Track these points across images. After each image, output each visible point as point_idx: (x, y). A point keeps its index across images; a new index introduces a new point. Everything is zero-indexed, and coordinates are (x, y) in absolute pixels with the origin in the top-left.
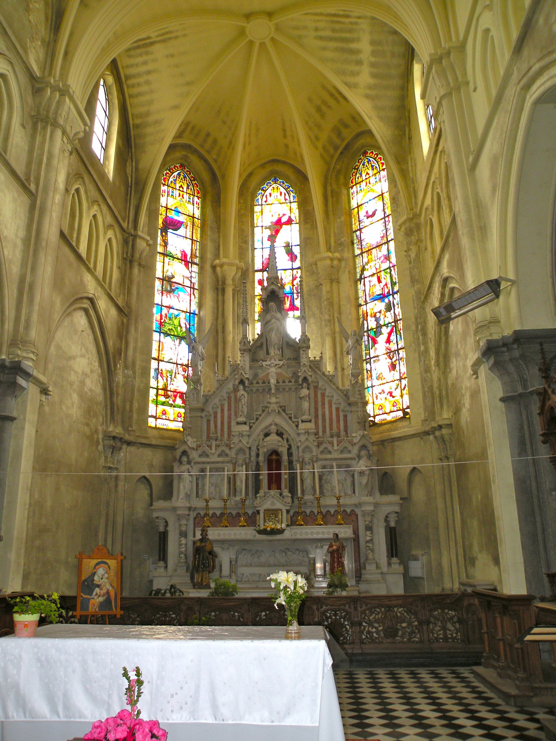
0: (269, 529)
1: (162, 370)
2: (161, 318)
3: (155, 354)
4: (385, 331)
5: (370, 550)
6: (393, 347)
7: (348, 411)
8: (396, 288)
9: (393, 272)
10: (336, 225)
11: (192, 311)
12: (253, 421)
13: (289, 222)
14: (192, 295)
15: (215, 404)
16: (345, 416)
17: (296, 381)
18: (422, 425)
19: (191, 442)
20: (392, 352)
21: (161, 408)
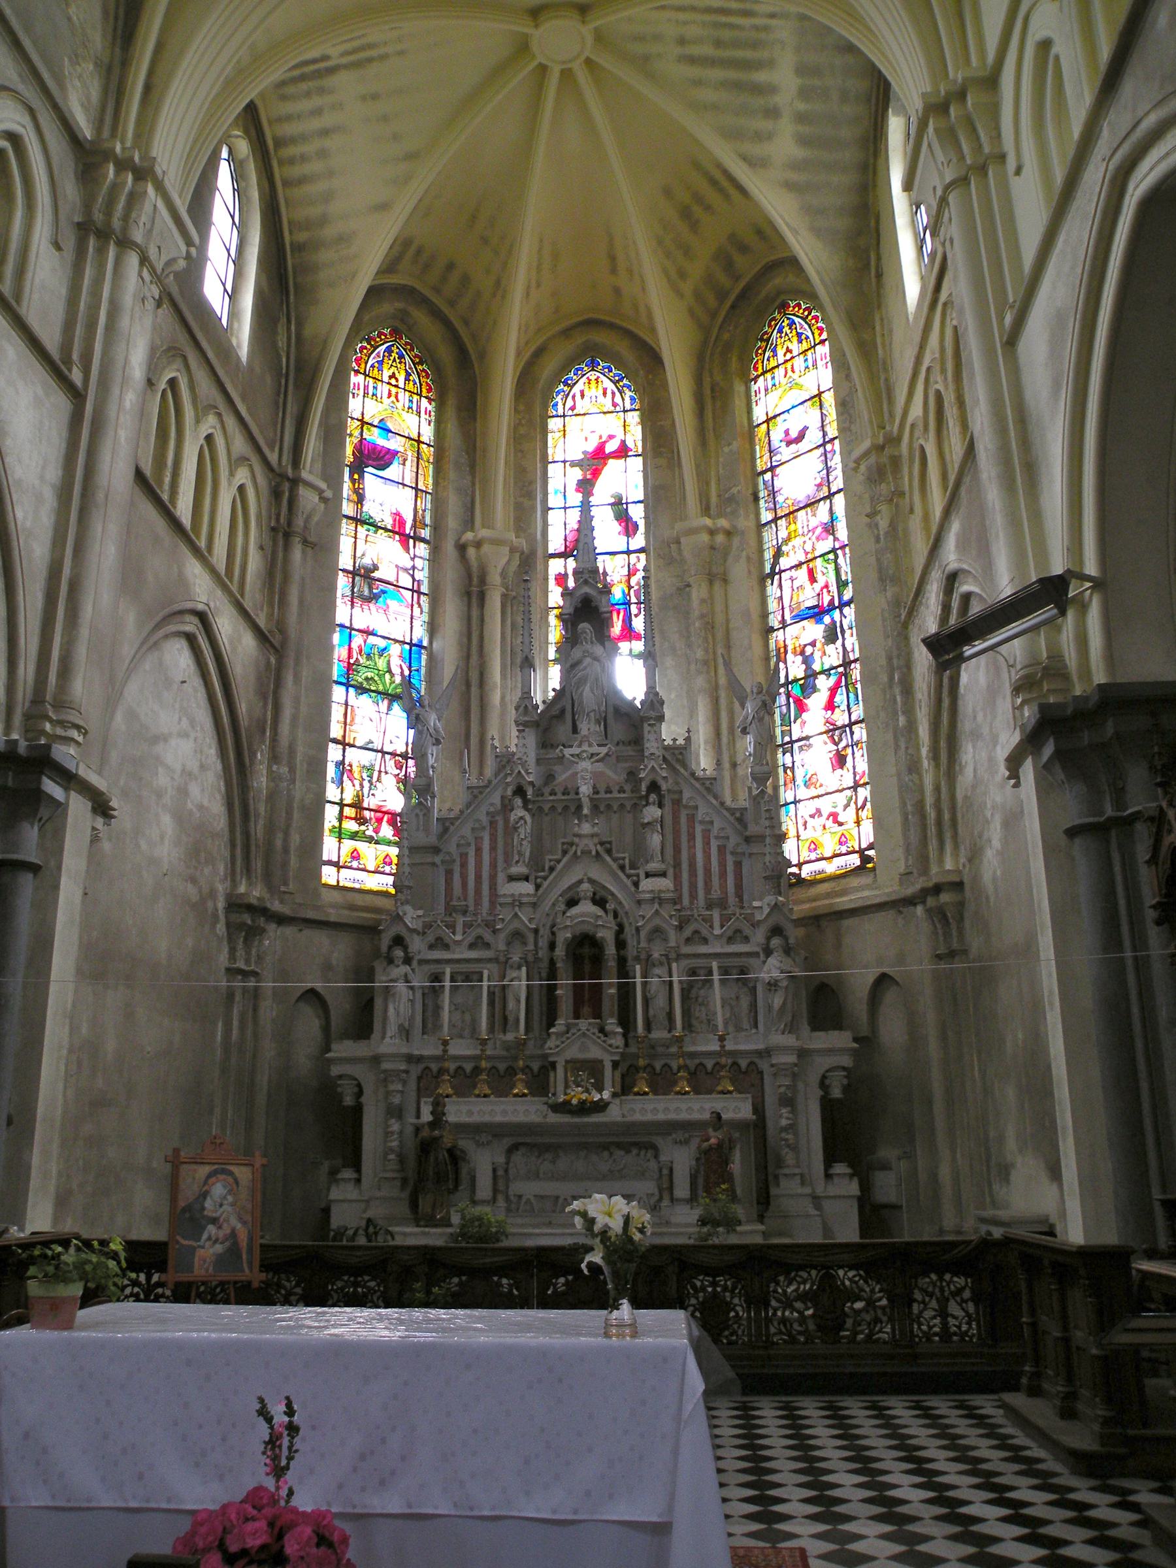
0: (574, 1101)
1: (350, 765)
2: (350, 656)
3: (336, 731)
4: (824, 684)
5: (788, 1146)
6: (841, 718)
8: (848, 594)
9: (841, 560)
10: (721, 460)
13: (623, 452)
14: (416, 606)
16: (738, 865)
17: (636, 789)
18: (901, 883)
19: (412, 917)
21: (348, 845)
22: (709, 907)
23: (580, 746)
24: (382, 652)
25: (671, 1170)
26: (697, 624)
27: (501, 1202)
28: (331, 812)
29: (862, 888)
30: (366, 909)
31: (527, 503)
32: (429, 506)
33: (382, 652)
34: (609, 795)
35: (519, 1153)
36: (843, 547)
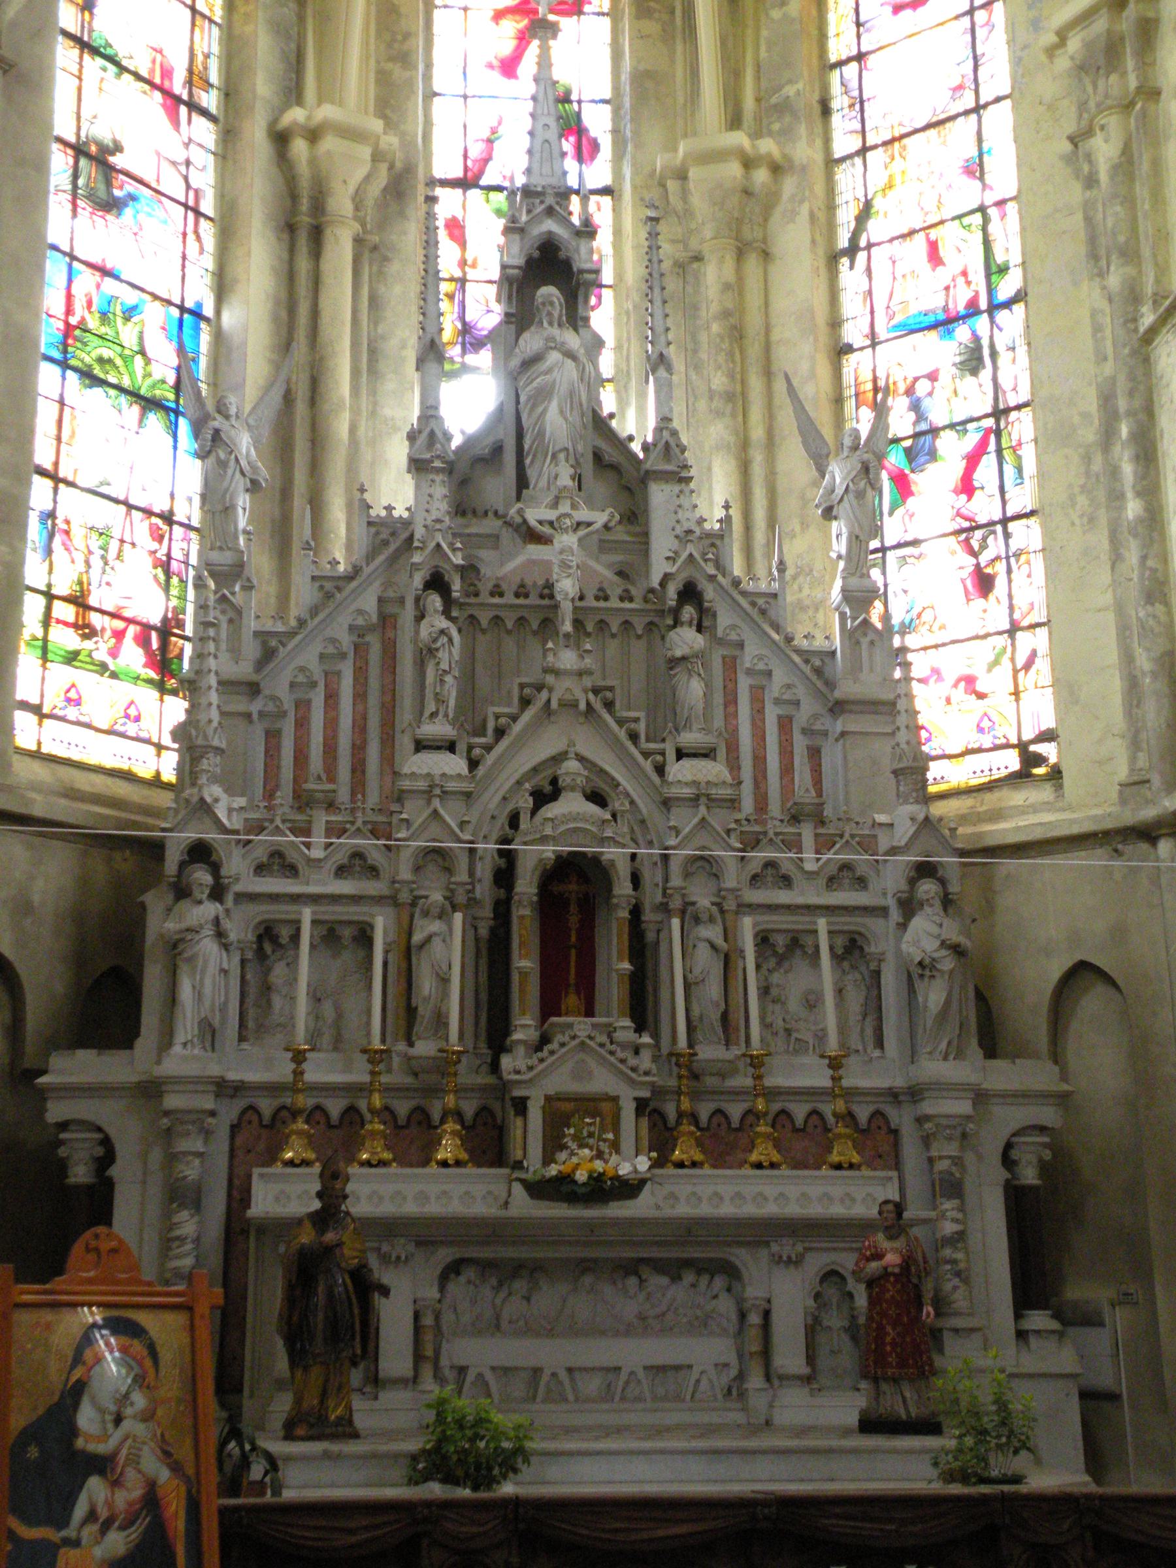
0: (581, 1176)
1: (67, 522)
2: (69, 311)
3: (43, 455)
5: (958, 1274)
6: (985, 507)
7: (825, 734)
9: (994, 228)
10: (764, 33)
11: (189, 304)
12: (482, 740)
14: (191, 237)
15: (302, 669)
16: (815, 753)
18: (1123, 801)
20: (978, 527)
21: (61, 675)
22: (795, 819)
23: (555, 504)
24: (129, 314)
25: (767, 1314)
26: (715, 328)
27: (427, 1372)
28: (33, 606)
29: (1035, 809)
30: (97, 799)
31: (396, 70)
32: (215, 49)
33: (129, 314)
34: (602, 604)
35: (462, 1279)
36: (1001, 203)
